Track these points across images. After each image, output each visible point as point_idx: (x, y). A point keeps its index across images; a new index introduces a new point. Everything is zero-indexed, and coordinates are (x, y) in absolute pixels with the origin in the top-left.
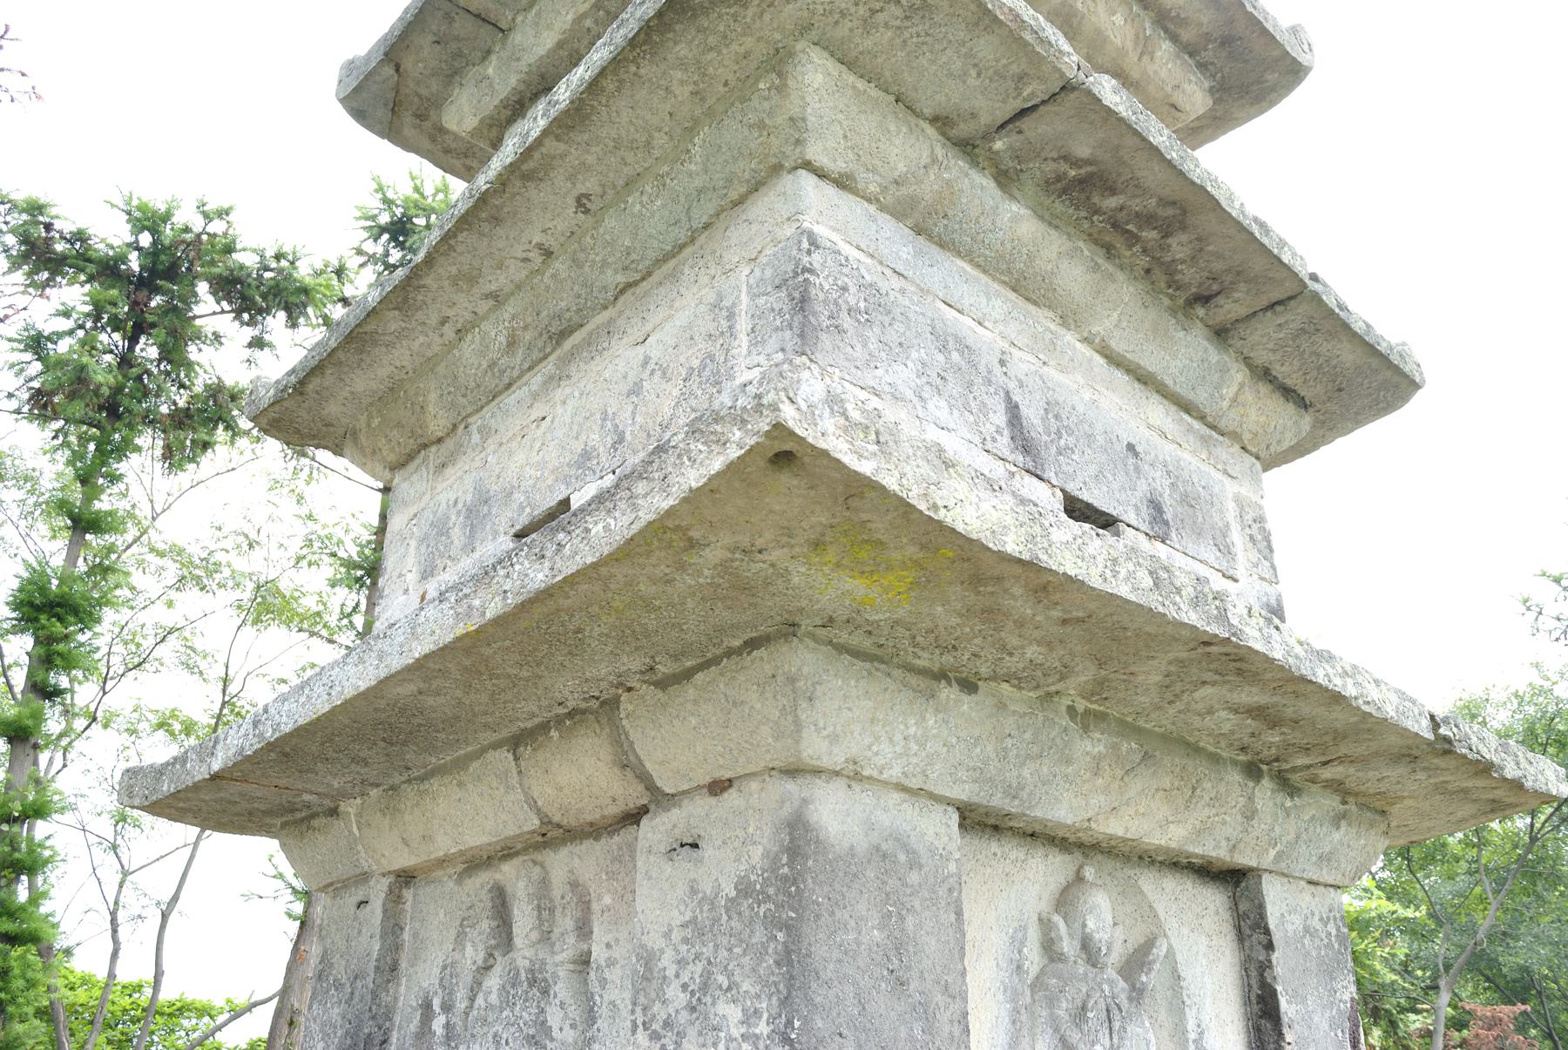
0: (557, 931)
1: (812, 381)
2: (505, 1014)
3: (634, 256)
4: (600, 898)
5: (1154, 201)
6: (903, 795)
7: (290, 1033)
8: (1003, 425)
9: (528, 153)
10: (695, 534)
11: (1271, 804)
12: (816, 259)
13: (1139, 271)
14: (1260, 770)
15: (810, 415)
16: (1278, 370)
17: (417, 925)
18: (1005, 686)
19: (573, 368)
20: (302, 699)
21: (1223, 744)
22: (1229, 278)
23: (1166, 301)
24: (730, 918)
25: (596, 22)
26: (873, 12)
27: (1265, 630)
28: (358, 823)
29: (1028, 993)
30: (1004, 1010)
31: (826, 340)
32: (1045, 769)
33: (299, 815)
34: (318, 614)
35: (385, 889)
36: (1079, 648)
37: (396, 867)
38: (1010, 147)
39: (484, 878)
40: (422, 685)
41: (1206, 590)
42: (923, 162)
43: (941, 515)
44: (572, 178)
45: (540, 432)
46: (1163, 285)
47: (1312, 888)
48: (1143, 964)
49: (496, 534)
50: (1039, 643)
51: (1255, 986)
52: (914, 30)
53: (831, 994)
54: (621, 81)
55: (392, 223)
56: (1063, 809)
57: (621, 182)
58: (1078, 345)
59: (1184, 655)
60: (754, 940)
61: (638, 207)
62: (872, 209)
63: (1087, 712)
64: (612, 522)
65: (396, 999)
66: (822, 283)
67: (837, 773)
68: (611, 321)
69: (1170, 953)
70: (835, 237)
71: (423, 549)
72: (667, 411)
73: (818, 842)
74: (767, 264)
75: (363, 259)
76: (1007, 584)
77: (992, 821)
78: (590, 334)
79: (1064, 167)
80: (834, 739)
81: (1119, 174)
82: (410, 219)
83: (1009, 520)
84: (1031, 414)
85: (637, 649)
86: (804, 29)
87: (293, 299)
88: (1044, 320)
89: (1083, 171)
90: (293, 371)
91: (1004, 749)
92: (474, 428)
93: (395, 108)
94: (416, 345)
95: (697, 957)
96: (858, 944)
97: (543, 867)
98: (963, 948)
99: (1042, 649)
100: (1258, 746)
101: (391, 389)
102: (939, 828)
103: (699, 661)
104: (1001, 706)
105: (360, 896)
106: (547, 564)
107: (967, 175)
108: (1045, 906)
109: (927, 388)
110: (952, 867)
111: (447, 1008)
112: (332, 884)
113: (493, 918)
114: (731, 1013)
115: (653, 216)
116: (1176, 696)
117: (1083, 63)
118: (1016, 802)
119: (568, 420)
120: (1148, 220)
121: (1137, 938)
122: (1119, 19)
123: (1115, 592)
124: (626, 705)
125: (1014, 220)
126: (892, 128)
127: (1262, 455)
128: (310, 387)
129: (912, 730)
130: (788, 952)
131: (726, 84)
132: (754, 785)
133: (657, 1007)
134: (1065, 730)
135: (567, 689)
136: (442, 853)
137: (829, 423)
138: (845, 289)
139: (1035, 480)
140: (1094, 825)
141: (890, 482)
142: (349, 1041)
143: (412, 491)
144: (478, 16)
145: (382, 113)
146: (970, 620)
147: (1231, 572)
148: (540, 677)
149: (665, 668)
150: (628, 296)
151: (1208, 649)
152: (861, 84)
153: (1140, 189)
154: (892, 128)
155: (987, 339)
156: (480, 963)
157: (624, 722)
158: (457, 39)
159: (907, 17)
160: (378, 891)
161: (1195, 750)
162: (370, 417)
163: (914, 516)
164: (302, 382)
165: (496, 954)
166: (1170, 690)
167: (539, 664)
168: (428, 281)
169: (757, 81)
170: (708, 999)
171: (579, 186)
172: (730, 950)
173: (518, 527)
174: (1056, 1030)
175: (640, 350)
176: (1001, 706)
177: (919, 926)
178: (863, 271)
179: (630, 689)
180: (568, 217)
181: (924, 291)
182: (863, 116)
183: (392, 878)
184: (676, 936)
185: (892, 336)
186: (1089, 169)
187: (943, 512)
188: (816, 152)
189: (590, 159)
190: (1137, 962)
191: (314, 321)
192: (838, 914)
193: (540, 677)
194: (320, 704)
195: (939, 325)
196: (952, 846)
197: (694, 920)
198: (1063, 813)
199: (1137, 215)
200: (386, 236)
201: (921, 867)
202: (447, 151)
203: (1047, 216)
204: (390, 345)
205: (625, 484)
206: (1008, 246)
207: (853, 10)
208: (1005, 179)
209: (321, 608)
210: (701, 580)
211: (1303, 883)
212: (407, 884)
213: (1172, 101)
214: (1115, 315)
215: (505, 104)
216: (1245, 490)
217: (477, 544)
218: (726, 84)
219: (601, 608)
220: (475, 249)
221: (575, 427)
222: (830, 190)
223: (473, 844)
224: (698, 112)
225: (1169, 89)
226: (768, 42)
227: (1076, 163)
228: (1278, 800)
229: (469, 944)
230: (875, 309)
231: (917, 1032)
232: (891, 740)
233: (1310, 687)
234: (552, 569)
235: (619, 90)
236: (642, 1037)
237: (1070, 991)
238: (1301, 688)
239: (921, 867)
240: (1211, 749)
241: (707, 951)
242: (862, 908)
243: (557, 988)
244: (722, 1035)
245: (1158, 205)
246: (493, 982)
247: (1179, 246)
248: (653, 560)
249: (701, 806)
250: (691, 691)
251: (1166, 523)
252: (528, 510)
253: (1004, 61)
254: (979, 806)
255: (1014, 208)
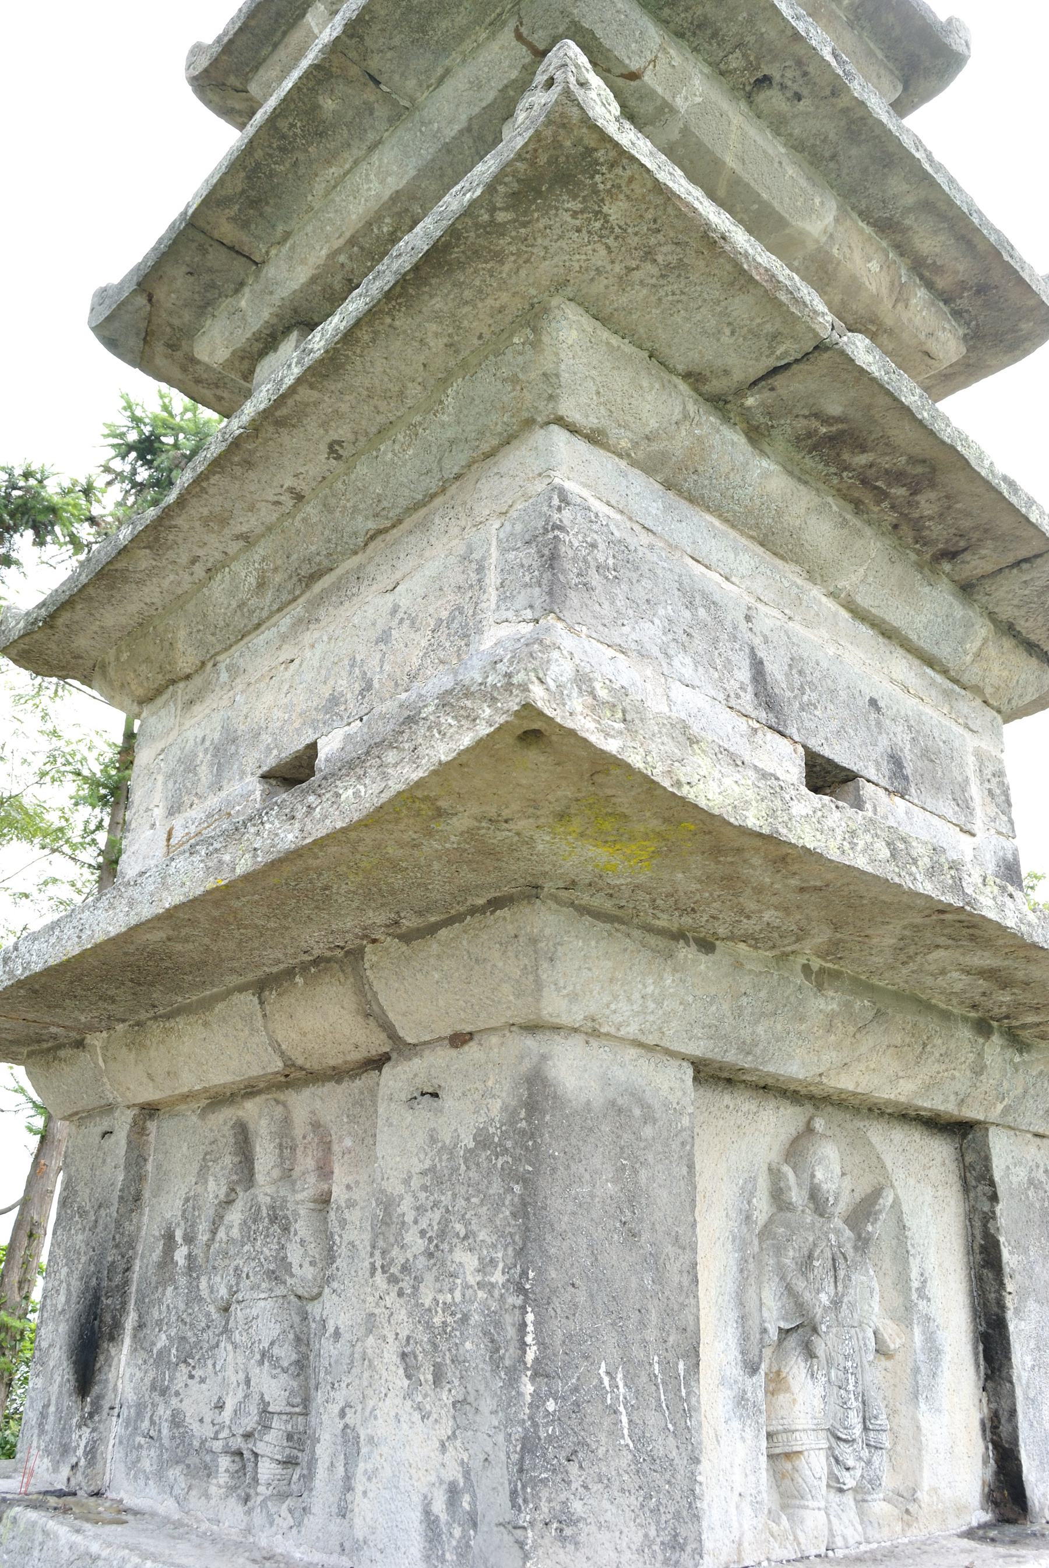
0: (298, 1169)
1: (561, 661)
2: (246, 1248)
3: (385, 504)
4: (341, 1139)
5: (903, 459)
6: (639, 1051)
7: (29, 1245)
8: (747, 681)
9: (281, 401)
10: (443, 804)
11: (1000, 1059)
12: (567, 514)
13: (887, 527)
14: (990, 1026)
15: (559, 696)
16: (1022, 625)
17: (161, 1156)
18: (742, 945)
19: (322, 612)
20: (53, 940)
21: (954, 1001)
22: (976, 536)
23: (913, 557)
24: (468, 1168)
25: (351, 258)
26: (629, 270)
27: (999, 899)
28: (104, 1056)
29: (756, 1242)
30: (732, 1260)
31: (574, 598)
32: (779, 1027)
33: (45, 1045)
34: (61, 830)
35: (130, 1120)
36: (815, 913)
37: (140, 1100)
38: (762, 404)
39: (226, 1115)
40: (171, 933)
41: (943, 860)
42: (675, 418)
43: (685, 791)
44: (324, 425)
45: (287, 675)
46: (910, 540)
47: (1038, 1140)
48: (869, 1214)
49: (243, 774)
50: (776, 908)
51: (978, 1237)
52: (669, 288)
53: (565, 1245)
54: (376, 333)
55: (140, 441)
56: (796, 1065)
57: (374, 430)
58: (824, 599)
59: (918, 920)
60: (491, 1192)
61: (390, 455)
62: (623, 464)
63: (822, 970)
64: (362, 788)
65: (139, 1229)
66: (572, 541)
67: (575, 1030)
68: (361, 567)
69: (896, 1203)
70: (585, 493)
71: (170, 785)
72: (416, 662)
73: (555, 1097)
74: (517, 519)
75: (109, 477)
76: (747, 855)
77: (725, 1075)
78: (340, 579)
79: (815, 424)
80: (573, 997)
81: (870, 432)
82: (158, 438)
83: (750, 795)
84: (775, 669)
85: (382, 905)
86: (560, 285)
87: (40, 518)
88: (791, 575)
89: (834, 429)
90: (43, 604)
91: (740, 1007)
92: (222, 666)
93: (148, 337)
94: (166, 583)
95: (436, 1204)
96: (592, 1196)
97: (285, 1106)
98: (694, 1200)
99: (780, 914)
100: (990, 1004)
101: (141, 624)
102: (674, 1083)
103: (443, 917)
104: (738, 965)
105: (105, 1126)
106: (297, 825)
107: (718, 431)
108: (774, 1156)
109: (673, 645)
110: (686, 1121)
111: (189, 1239)
112: (77, 1113)
113: (236, 1154)
114: (467, 1261)
115: (404, 464)
116: (910, 957)
117: (838, 323)
118: (750, 1058)
119: (316, 664)
120: (897, 477)
121: (864, 1188)
122: (874, 266)
123: (852, 863)
124: (371, 955)
125: (763, 476)
126: (645, 384)
127: (1003, 708)
128: (60, 622)
129: (650, 989)
130: (525, 1205)
131: (480, 337)
132: (494, 1040)
133: (395, 1252)
134: (800, 988)
135: (314, 939)
136: (186, 1090)
137: (577, 703)
138: (594, 546)
139: (777, 736)
140: (825, 1080)
141: (636, 760)
142: (92, 1268)
143: (160, 726)
144: (231, 248)
145: (134, 342)
146: (706, 886)
147: (968, 827)
148: (287, 929)
149: (409, 922)
150: (378, 542)
151: (942, 917)
152: (615, 340)
153: (890, 447)
154: (645, 384)
155: (733, 594)
156: (222, 1197)
157: (368, 972)
158: (210, 270)
159: (663, 276)
160: (123, 1122)
161: (927, 1007)
162: (119, 651)
163: (657, 793)
164: (52, 616)
165: (238, 1189)
166: (904, 951)
167: (286, 917)
168: (179, 521)
169: (511, 336)
170: (445, 1246)
171: (331, 432)
172: (468, 1199)
173: (265, 769)
174: (783, 1278)
175: (390, 598)
176: (738, 965)
177: (652, 1179)
178: (613, 528)
179: (374, 941)
180: (320, 463)
181: (672, 547)
182: (616, 372)
183: (136, 1111)
184: (416, 1183)
185: (640, 593)
186: (840, 426)
187: (686, 788)
188: (568, 408)
189: (344, 407)
190: (863, 1212)
191: (62, 539)
192: (574, 1167)
193: (287, 929)
194: (70, 947)
195: (686, 581)
196: (686, 1101)
197: (432, 1169)
198: (795, 1068)
199: (887, 472)
200: (133, 455)
201: (655, 1121)
202: (198, 381)
203: (797, 472)
204: (141, 582)
205: (375, 752)
206: (758, 502)
207: (609, 267)
208: (756, 434)
209: (64, 823)
210: (448, 845)
211: (1029, 1136)
212: (151, 1116)
213: (925, 348)
214: (862, 570)
215: (257, 337)
216: (985, 744)
217: (224, 783)
218: (480, 337)
219: (349, 867)
220: (227, 492)
221: (323, 672)
222: (582, 446)
223: (217, 1082)
224: (452, 363)
225: (922, 337)
226: (523, 298)
227: (827, 420)
228: (1008, 1056)
229: (211, 1178)
230: (626, 564)
231: (648, 1282)
232: (629, 999)
233: (1042, 954)
234: (302, 831)
235: (373, 340)
236: (380, 1279)
237: (797, 1241)
238: (1033, 954)
239: (655, 1121)
240: (943, 1006)
241: (446, 1199)
242: (596, 1161)
243: (297, 1226)
244: (458, 1281)
245: (908, 463)
246: (235, 1216)
247: (927, 504)
248: (402, 826)
249: (441, 1058)
250: (435, 946)
251: (906, 778)
252: (275, 752)
253: (759, 321)
254: (712, 1061)
255: (765, 463)
